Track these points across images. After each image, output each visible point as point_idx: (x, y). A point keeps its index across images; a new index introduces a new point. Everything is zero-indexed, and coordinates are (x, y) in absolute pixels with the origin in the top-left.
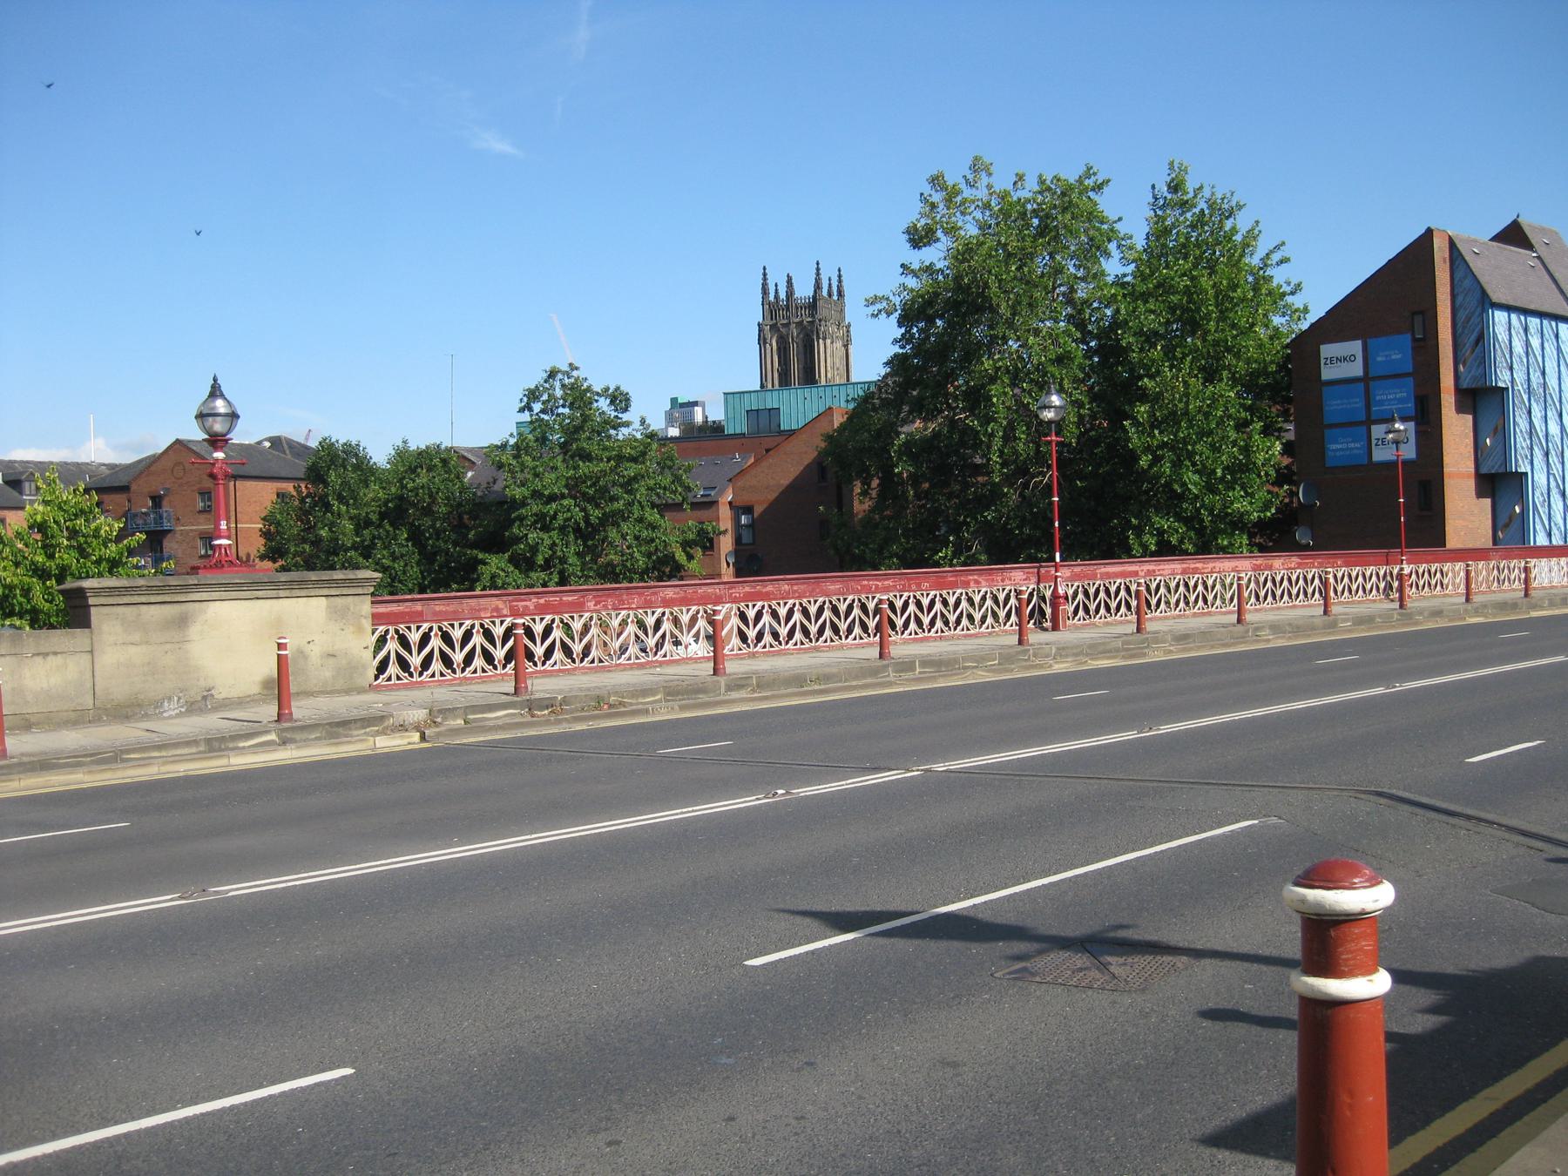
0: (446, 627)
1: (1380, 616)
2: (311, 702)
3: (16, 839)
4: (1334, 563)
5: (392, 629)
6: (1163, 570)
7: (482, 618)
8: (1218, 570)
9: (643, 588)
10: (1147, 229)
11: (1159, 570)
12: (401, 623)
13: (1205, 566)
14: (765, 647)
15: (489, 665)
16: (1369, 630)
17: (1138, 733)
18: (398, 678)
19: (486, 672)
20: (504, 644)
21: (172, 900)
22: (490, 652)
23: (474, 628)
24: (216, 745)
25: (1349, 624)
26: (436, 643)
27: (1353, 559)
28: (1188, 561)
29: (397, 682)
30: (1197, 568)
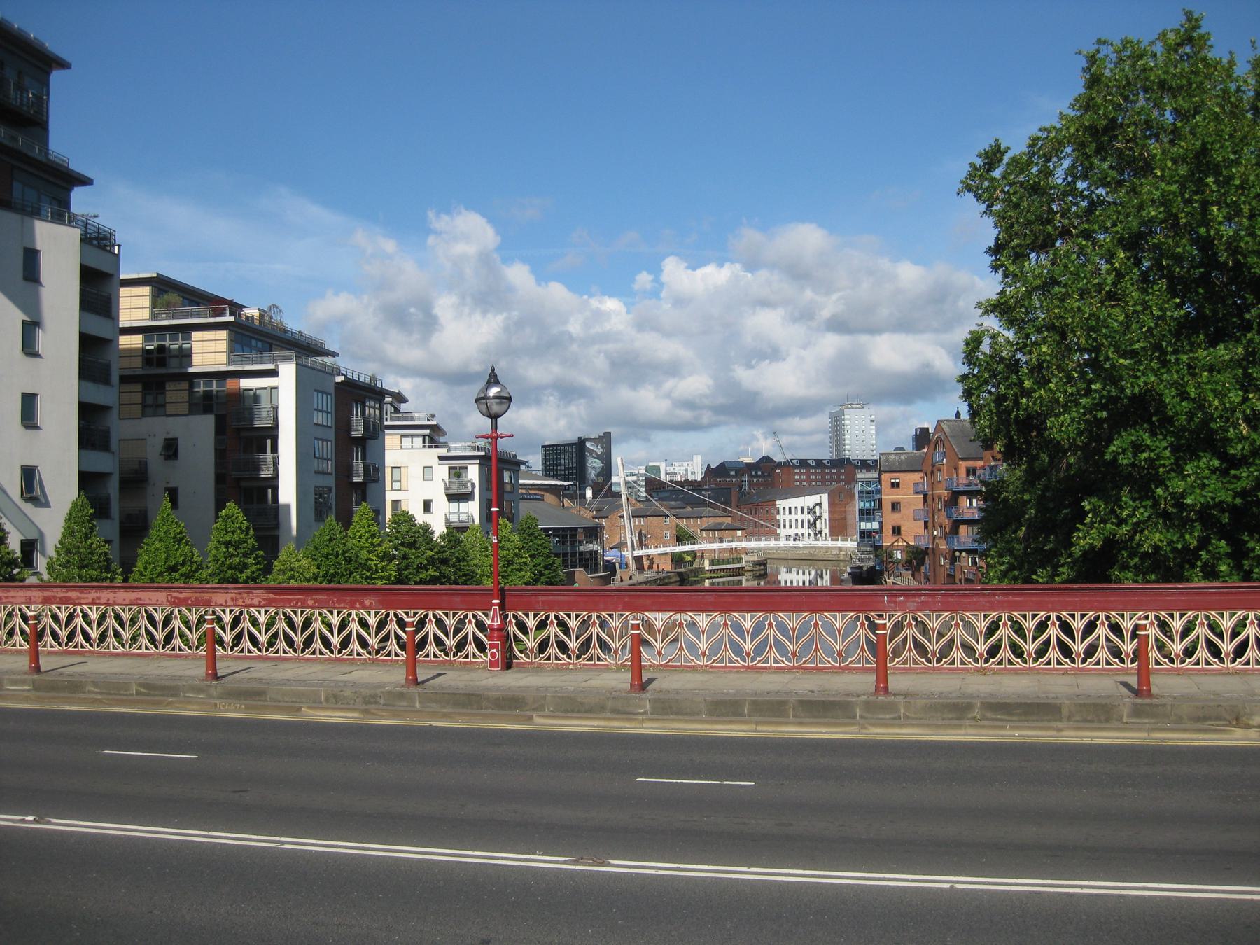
0: (1065, 617)
1: (95, 684)
2: (222, 671)
3: (675, 781)
4: (355, 602)
5: (1053, 616)
6: (13, 597)
7: (81, 604)
8: (103, 601)
9: (953, 590)
10: (988, 233)
11: (7, 597)
12: (1113, 610)
13: (83, 595)
14: (1001, 662)
15: (563, 654)
16: (249, 708)
17: (35, 821)
18: (435, 656)
19: (398, 656)
20: (426, 636)
21: (564, 862)
22: (365, 640)
23: (1247, 619)
24: (372, 700)
25: (26, 688)
26: (1053, 631)
27: (562, 598)
28: (1025, 594)
29: (1056, 666)
30: (70, 598)
